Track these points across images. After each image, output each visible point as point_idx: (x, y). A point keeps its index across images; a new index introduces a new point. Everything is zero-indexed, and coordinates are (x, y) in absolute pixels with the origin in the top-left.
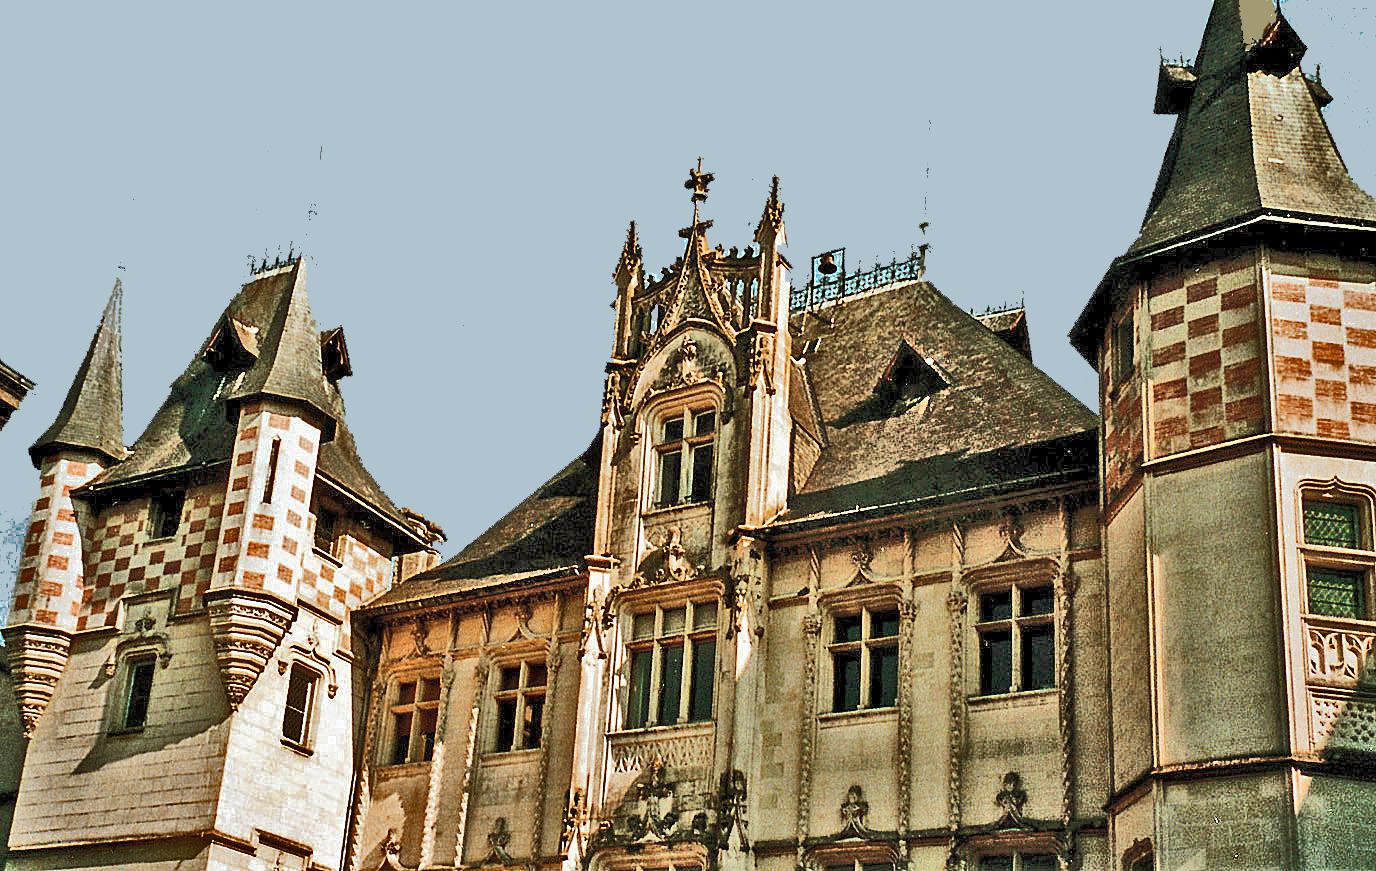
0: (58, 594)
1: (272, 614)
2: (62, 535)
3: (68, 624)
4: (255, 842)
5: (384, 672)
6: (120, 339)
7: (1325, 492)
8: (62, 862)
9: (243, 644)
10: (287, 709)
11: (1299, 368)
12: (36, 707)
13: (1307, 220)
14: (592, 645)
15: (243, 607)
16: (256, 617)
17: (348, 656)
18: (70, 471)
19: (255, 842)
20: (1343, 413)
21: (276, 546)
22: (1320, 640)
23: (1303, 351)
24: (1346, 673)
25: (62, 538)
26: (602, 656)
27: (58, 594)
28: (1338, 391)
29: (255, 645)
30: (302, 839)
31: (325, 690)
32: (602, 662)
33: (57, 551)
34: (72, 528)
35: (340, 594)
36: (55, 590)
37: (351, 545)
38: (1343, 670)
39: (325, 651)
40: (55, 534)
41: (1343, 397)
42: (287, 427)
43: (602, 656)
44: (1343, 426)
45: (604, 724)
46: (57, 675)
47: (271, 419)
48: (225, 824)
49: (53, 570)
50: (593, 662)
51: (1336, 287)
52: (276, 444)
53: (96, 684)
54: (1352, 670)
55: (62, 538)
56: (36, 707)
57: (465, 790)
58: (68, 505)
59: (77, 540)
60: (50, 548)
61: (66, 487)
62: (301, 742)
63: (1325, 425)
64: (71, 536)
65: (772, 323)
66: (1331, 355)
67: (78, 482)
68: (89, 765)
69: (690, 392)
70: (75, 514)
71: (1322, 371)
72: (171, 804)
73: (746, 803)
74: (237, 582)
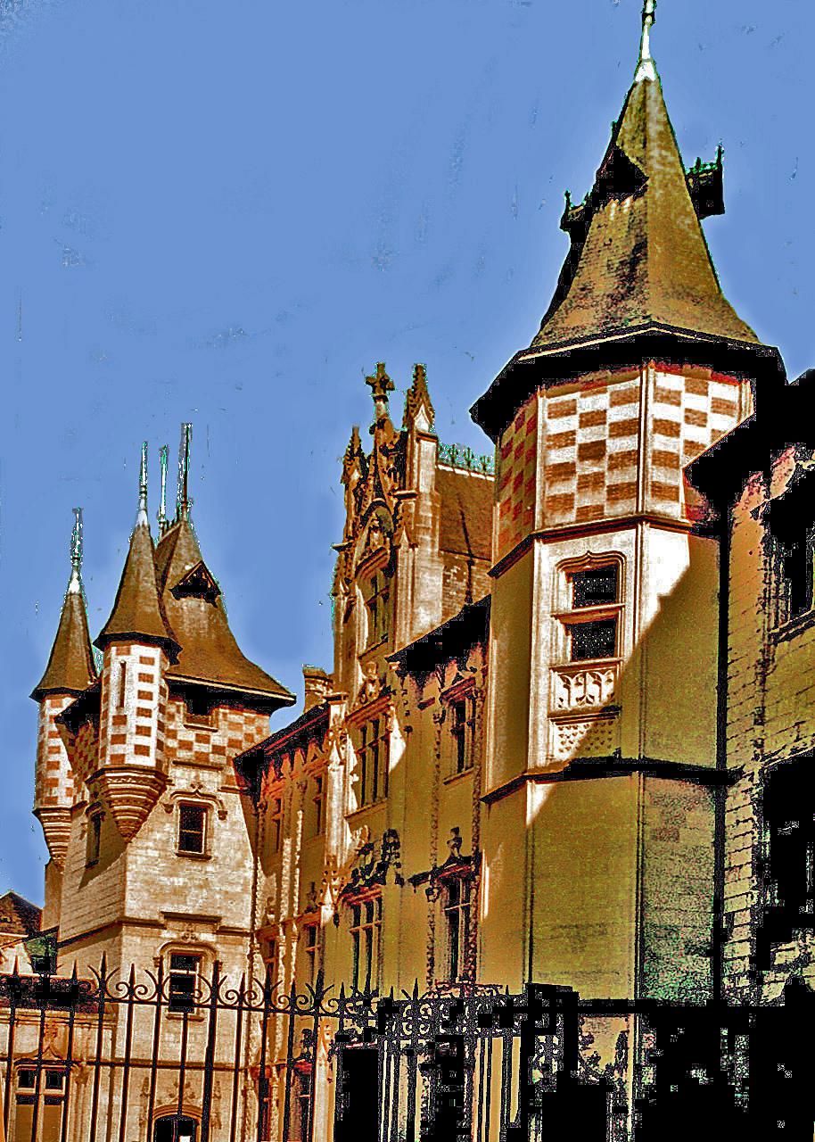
0: (56, 785)
1: (134, 778)
2: (53, 747)
3: (66, 802)
4: (162, 920)
5: (264, 794)
6: (82, 604)
7: (584, 565)
8: (83, 943)
9: (120, 800)
10: (181, 832)
11: (565, 471)
12: (59, 856)
13: (540, 352)
14: (334, 755)
15: (114, 778)
16: (124, 782)
17: (237, 790)
18: (53, 706)
19: (162, 920)
20: (599, 498)
21: (131, 734)
22: (599, 678)
23: (568, 455)
24: (588, 702)
25: (57, 750)
26: (341, 763)
27: (56, 785)
28: (596, 481)
29: (128, 800)
30: (210, 912)
31: (215, 816)
32: (342, 767)
33: (54, 758)
34: (59, 742)
35: (218, 750)
36: (55, 782)
37: (225, 714)
38: (584, 699)
39: (211, 789)
40: (49, 748)
41: (601, 484)
42: (128, 653)
43: (341, 763)
44: (600, 508)
45: (344, 807)
46: (68, 834)
47: (117, 650)
48: (133, 908)
49: (50, 772)
50: (336, 768)
51: (605, 391)
52: (123, 665)
53: (82, 836)
54: (592, 697)
55: (57, 750)
56: (59, 856)
57: (297, 866)
58: (54, 728)
59: (63, 749)
60: (47, 757)
61: (51, 717)
62: (203, 853)
63: (583, 512)
64: (59, 747)
65: (413, 491)
66: (593, 451)
67: (57, 711)
68: (84, 884)
69: (376, 558)
70: (59, 732)
71: (589, 468)
72: (734, 897)
73: (399, 851)
74: (107, 763)
